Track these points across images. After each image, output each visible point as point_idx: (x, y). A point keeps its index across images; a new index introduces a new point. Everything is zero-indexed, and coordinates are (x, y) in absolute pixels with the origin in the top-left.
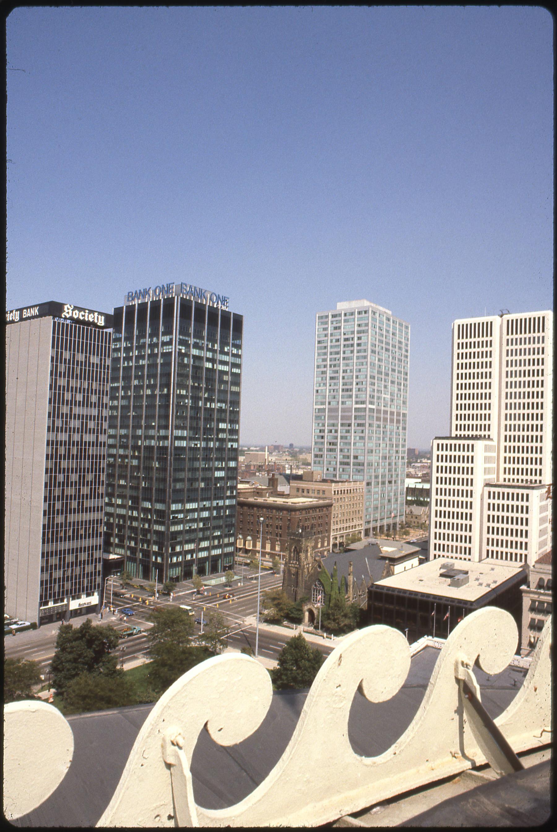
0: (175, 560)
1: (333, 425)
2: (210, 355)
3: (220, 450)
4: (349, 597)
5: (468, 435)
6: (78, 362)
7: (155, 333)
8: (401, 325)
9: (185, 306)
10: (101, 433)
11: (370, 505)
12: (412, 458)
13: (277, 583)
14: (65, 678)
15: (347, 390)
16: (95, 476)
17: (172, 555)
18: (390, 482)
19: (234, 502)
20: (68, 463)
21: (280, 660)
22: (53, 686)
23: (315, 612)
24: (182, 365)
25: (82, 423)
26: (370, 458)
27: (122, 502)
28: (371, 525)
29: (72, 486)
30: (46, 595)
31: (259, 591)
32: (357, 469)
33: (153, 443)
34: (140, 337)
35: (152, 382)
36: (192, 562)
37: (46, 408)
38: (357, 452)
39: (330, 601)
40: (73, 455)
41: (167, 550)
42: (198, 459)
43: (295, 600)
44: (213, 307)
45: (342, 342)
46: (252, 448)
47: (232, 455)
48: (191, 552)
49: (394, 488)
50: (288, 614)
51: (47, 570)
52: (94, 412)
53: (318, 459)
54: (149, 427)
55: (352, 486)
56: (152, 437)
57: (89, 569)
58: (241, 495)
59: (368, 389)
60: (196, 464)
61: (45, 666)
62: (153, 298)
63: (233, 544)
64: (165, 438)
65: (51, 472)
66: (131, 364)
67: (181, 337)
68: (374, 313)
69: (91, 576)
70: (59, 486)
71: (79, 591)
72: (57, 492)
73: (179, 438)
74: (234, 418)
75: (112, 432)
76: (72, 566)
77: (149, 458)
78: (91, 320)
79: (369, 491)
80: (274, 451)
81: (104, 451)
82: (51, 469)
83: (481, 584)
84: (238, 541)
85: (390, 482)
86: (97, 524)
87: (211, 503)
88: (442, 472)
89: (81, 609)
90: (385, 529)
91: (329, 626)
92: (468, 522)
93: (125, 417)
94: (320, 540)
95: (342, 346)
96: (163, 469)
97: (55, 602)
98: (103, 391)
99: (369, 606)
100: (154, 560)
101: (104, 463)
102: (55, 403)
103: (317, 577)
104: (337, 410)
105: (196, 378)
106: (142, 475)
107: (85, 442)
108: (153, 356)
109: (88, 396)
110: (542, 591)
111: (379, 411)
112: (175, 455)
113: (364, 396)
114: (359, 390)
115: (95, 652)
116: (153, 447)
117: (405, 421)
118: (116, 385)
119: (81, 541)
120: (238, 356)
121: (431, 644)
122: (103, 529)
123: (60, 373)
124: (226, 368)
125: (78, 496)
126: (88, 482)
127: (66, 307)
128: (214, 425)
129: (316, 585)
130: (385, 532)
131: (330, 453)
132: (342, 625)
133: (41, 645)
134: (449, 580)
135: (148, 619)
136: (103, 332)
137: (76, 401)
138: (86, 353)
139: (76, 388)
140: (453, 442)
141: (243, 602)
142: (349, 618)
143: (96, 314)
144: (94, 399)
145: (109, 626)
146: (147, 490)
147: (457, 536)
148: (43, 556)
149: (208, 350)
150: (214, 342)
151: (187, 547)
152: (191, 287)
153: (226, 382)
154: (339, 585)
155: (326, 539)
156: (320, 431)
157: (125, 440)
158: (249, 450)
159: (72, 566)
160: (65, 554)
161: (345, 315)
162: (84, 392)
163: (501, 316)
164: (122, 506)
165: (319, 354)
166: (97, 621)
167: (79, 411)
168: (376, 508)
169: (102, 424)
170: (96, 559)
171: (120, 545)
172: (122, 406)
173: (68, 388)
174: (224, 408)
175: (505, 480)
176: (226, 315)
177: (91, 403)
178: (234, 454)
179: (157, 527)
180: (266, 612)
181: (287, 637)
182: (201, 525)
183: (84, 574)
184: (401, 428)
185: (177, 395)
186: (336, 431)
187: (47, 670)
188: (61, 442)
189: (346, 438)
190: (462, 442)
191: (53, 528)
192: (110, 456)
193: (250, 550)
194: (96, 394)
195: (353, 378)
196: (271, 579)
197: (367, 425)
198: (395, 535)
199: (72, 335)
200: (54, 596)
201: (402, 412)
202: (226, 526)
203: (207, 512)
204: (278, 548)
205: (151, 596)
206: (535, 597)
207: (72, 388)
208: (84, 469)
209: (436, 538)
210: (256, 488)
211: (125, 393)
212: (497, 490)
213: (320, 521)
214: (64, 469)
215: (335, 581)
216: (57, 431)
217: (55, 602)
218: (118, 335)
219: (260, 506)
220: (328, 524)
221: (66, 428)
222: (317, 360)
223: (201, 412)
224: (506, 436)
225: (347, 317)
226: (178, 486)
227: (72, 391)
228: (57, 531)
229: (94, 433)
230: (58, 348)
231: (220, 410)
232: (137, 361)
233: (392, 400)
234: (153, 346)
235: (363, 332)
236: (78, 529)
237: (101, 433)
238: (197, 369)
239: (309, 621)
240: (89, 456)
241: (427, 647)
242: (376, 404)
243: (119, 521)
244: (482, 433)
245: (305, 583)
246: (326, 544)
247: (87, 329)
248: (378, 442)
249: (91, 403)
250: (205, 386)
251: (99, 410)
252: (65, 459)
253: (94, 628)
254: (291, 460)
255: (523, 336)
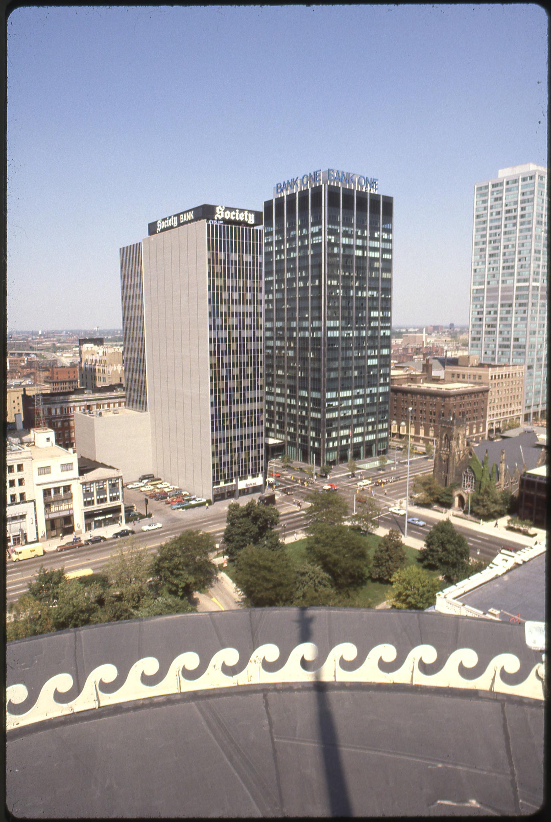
0: (331, 445)
1: (492, 306)
2: (359, 242)
3: (373, 338)
4: (500, 485)
9: (333, 193)
10: (258, 328)
11: (531, 390)
13: (428, 468)
14: (235, 547)
15: (508, 268)
16: (254, 369)
17: (328, 441)
19: (387, 389)
20: (230, 358)
21: (427, 542)
23: (465, 497)
24: (331, 255)
25: (240, 320)
26: (533, 339)
27: (281, 391)
28: (532, 410)
30: (217, 476)
31: (408, 476)
32: (517, 352)
33: (307, 334)
34: (290, 229)
35: (304, 275)
37: (207, 308)
38: (518, 334)
39: (480, 488)
41: (324, 436)
42: (351, 349)
44: (361, 192)
46: (410, 330)
48: (347, 437)
50: (438, 499)
51: (217, 455)
52: (250, 309)
53: (476, 342)
55: (511, 370)
56: (306, 329)
57: (253, 453)
58: (395, 382)
59: (532, 265)
60: (349, 353)
61: (219, 537)
63: (387, 430)
64: (319, 329)
65: (215, 367)
66: (283, 257)
67: (330, 227)
71: (246, 473)
72: (222, 385)
73: (333, 328)
74: (387, 305)
76: (238, 451)
77: (304, 349)
78: (242, 219)
79: (531, 375)
81: (261, 345)
87: (365, 391)
89: (248, 489)
91: (479, 511)
93: (280, 310)
94: (475, 426)
95: (503, 219)
96: (317, 359)
97: (226, 482)
99: (521, 493)
102: (214, 303)
103: (468, 464)
104: (496, 290)
105: (347, 267)
108: (304, 248)
109: (243, 294)
112: (329, 345)
114: (521, 267)
115: (259, 527)
116: (307, 338)
120: (389, 241)
122: (264, 416)
124: (376, 255)
125: (240, 388)
127: (217, 209)
128: (365, 313)
129: (466, 472)
131: (489, 336)
133: (215, 519)
135: (306, 500)
136: (253, 230)
138: (239, 252)
143: (246, 212)
144: (249, 296)
146: (303, 379)
149: (358, 237)
151: (343, 433)
152: (338, 173)
153: (377, 269)
154: (490, 472)
155: (482, 425)
156: (478, 313)
157: (281, 333)
158: (407, 332)
159: (238, 451)
160: (231, 440)
162: (240, 291)
164: (281, 395)
165: (477, 230)
167: (236, 309)
170: (259, 445)
171: (281, 431)
172: (276, 300)
174: (375, 295)
176: (375, 199)
177: (247, 300)
178: (386, 342)
179: (313, 415)
180: (416, 496)
181: (436, 520)
182: (355, 412)
186: (496, 312)
187: (221, 540)
189: (506, 319)
191: (220, 417)
192: (268, 347)
193: (404, 436)
194: (250, 291)
200: (225, 477)
202: (380, 413)
204: (431, 434)
210: (410, 375)
211: (278, 286)
213: (475, 407)
215: (486, 469)
217: (226, 482)
218: (269, 229)
219: (414, 393)
220: (484, 410)
221: (225, 326)
223: (352, 301)
225: (510, 186)
226: (333, 375)
227: (229, 290)
228: (223, 421)
229: (251, 329)
231: (372, 298)
232: (289, 254)
234: (303, 238)
235: (528, 201)
236: (241, 418)
237: (258, 328)
238: (347, 257)
239: (459, 506)
240: (247, 350)
243: (279, 409)
246: (481, 430)
249: (247, 300)
250: (355, 274)
254: (451, 341)
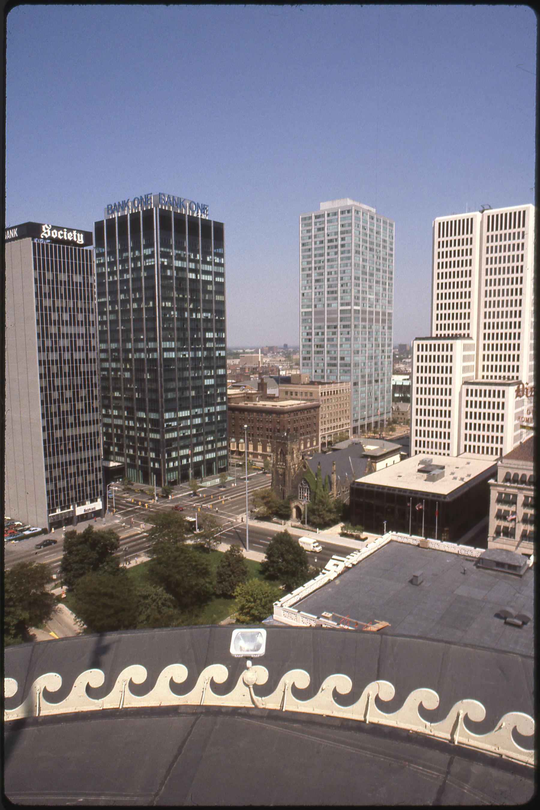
1: (320, 328)
2: (192, 266)
3: (208, 359)
4: (333, 494)
5: (449, 335)
6: (61, 281)
7: (136, 247)
8: (385, 222)
9: (165, 216)
10: (91, 350)
12: (403, 354)
13: (266, 483)
14: (74, 576)
15: (332, 292)
17: (168, 461)
18: (377, 381)
19: (225, 408)
22: (65, 585)
23: (302, 509)
24: (165, 278)
25: (71, 341)
27: (119, 413)
28: (359, 424)
29: (67, 402)
31: (247, 491)
32: (344, 370)
33: (143, 355)
35: (138, 296)
36: (187, 466)
37: (35, 329)
40: (65, 373)
43: (284, 498)
44: (192, 216)
45: (326, 244)
47: (220, 363)
48: (187, 457)
49: (380, 386)
50: (277, 511)
54: (138, 340)
55: (338, 387)
56: (141, 350)
57: (91, 477)
60: (186, 374)
62: (132, 211)
64: (155, 350)
66: (116, 279)
67: (162, 249)
68: (357, 212)
69: (93, 484)
70: (55, 403)
73: (169, 350)
74: (221, 327)
75: (103, 346)
77: (140, 371)
78: (70, 239)
79: (357, 391)
80: (269, 352)
82: (46, 387)
83: (455, 478)
84: (231, 444)
85: (377, 381)
86: (94, 436)
88: (422, 372)
90: (373, 425)
92: (447, 419)
93: (114, 332)
94: (309, 440)
98: (89, 309)
99: (351, 501)
100: (152, 466)
101: (95, 379)
102: (42, 324)
103: (303, 477)
104: (322, 313)
105: (181, 289)
106: (134, 386)
107: (76, 360)
108: (136, 270)
109: (74, 315)
110: (508, 484)
111: (364, 312)
112: (165, 366)
113: (349, 297)
114: (344, 292)
116: (143, 359)
117: (390, 320)
118: (103, 300)
119: (81, 453)
121: (395, 538)
123: (45, 294)
124: (209, 278)
125: (74, 411)
126: (82, 397)
127: (44, 227)
128: (200, 335)
129: (302, 484)
130: (373, 429)
132: (327, 519)
134: (425, 475)
136: (83, 250)
137: (63, 321)
139: (62, 308)
140: (433, 342)
141: (235, 501)
142: (334, 512)
143: (75, 232)
144: (80, 317)
145: (110, 530)
146: (141, 401)
147: (437, 432)
148: (46, 469)
149: (191, 261)
150: (196, 252)
151: (183, 452)
152: (169, 197)
153: (210, 292)
155: (315, 439)
156: (308, 334)
157: (116, 354)
158: (244, 352)
159: (75, 476)
160: (66, 465)
161: (328, 215)
163: (482, 212)
164: (118, 417)
165: (304, 257)
166: (99, 525)
168: (363, 407)
169: (90, 341)
170: (96, 469)
172: (110, 321)
173: (54, 308)
174: (209, 317)
175: (483, 377)
176: (206, 224)
177: (78, 321)
178: (222, 363)
179: (152, 436)
180: (256, 510)
182: (194, 431)
183: (86, 483)
184: (386, 328)
185: (162, 307)
186: (323, 334)
187: (59, 570)
188: (53, 361)
190: (441, 342)
191: (53, 442)
195: (337, 280)
196: (263, 479)
197: (353, 326)
198: (382, 431)
199: (54, 255)
200: (61, 504)
201: (387, 311)
202: (218, 431)
203: (199, 419)
204: (269, 449)
205: (151, 499)
206: (502, 489)
207: (58, 308)
208: (77, 385)
209: (416, 435)
210: (247, 393)
211: (112, 307)
212: (474, 387)
213: (308, 422)
214: (58, 386)
216: (48, 351)
219: (251, 411)
220: (316, 424)
221: (56, 348)
222: (301, 263)
224: (485, 334)
225: (331, 218)
226: (170, 395)
227: (58, 311)
228: (57, 445)
230: (40, 269)
231: (206, 320)
233: (377, 300)
234: (136, 259)
235: (347, 232)
236: (76, 442)
237: (91, 350)
238: (181, 280)
240: (80, 373)
241: (391, 541)
242: (361, 304)
244: (462, 332)
245: (292, 483)
246: (315, 444)
247: (67, 248)
248: (364, 342)
249: (78, 321)
250: (189, 297)
251: (86, 328)
252: (57, 377)
253: (96, 533)
254: (285, 361)
255: (503, 232)
